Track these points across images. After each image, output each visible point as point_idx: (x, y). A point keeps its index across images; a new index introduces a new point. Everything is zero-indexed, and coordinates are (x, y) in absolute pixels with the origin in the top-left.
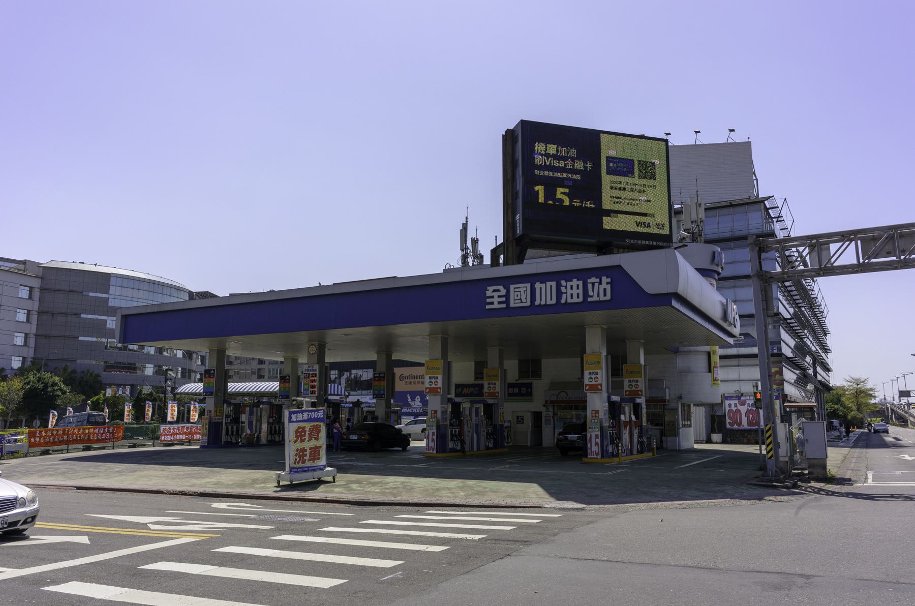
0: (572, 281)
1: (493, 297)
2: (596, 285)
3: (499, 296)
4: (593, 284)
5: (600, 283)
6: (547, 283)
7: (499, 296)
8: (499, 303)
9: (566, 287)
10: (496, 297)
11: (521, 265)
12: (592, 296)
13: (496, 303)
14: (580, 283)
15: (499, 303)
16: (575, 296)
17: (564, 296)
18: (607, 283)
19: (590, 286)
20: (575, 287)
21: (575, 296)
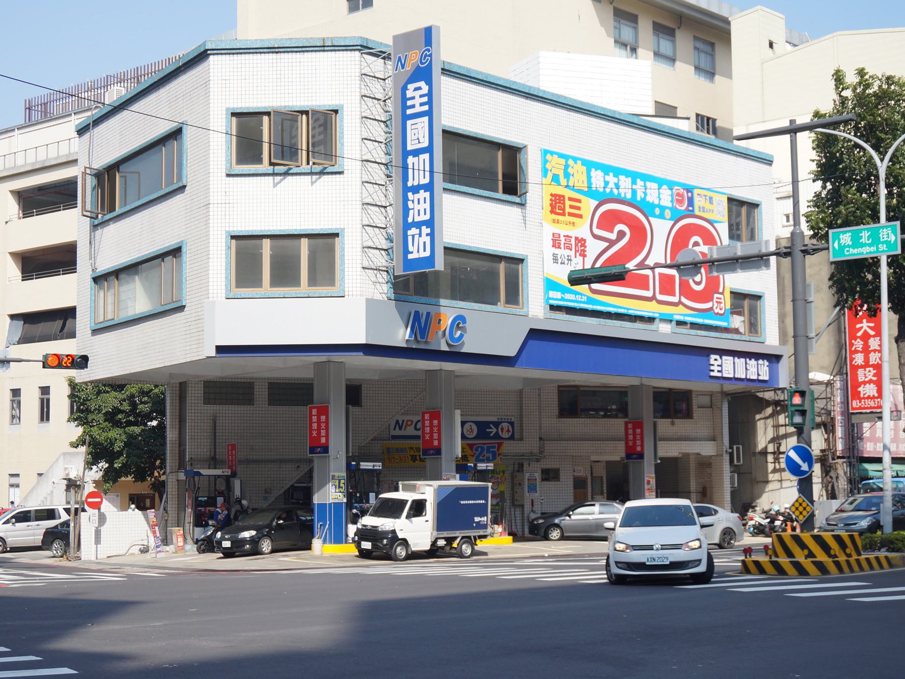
0: (419, 193)
1: (413, 98)
2: (416, 237)
3: (421, 96)
4: (413, 236)
5: (420, 235)
6: (420, 156)
7: (421, 96)
8: (422, 104)
9: (413, 201)
10: (417, 97)
11: (441, 28)
12: (412, 253)
13: (417, 105)
15: (422, 104)
16: (422, 212)
17: (411, 212)
18: (427, 235)
19: (410, 238)
20: (422, 201)
21: (422, 212)
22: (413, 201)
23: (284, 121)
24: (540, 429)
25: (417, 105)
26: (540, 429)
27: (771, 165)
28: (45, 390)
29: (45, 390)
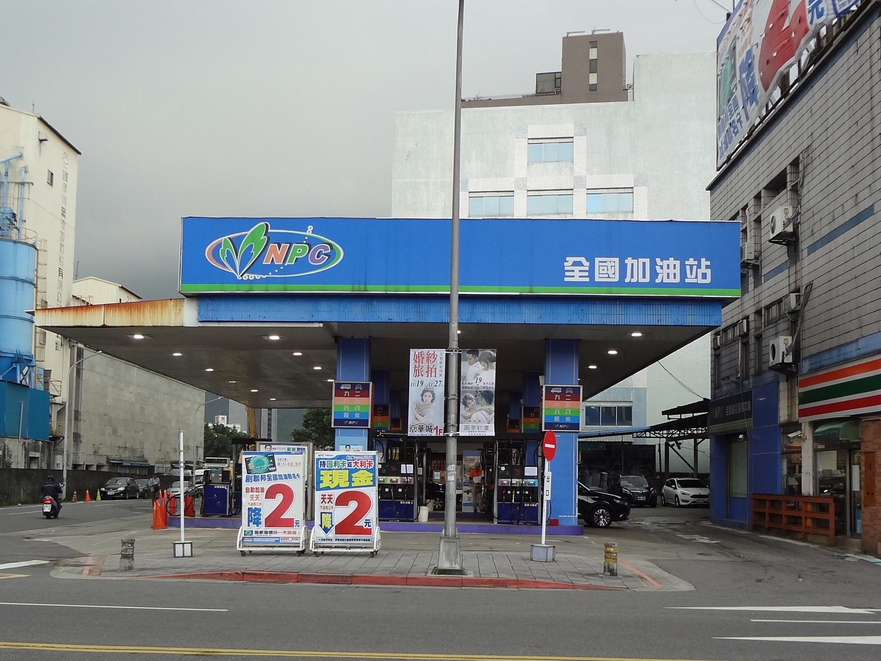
2: (695, 267)
4: (691, 266)
5: (699, 266)
9: (662, 267)
14: (678, 263)
18: (707, 267)
19: (688, 268)
20: (672, 267)
22: (662, 267)
23: (323, 514)
24: (10, 311)
25: (675, 271)
26: (10, 311)
27: (645, 263)
28: (632, 264)
29: (632, 264)
